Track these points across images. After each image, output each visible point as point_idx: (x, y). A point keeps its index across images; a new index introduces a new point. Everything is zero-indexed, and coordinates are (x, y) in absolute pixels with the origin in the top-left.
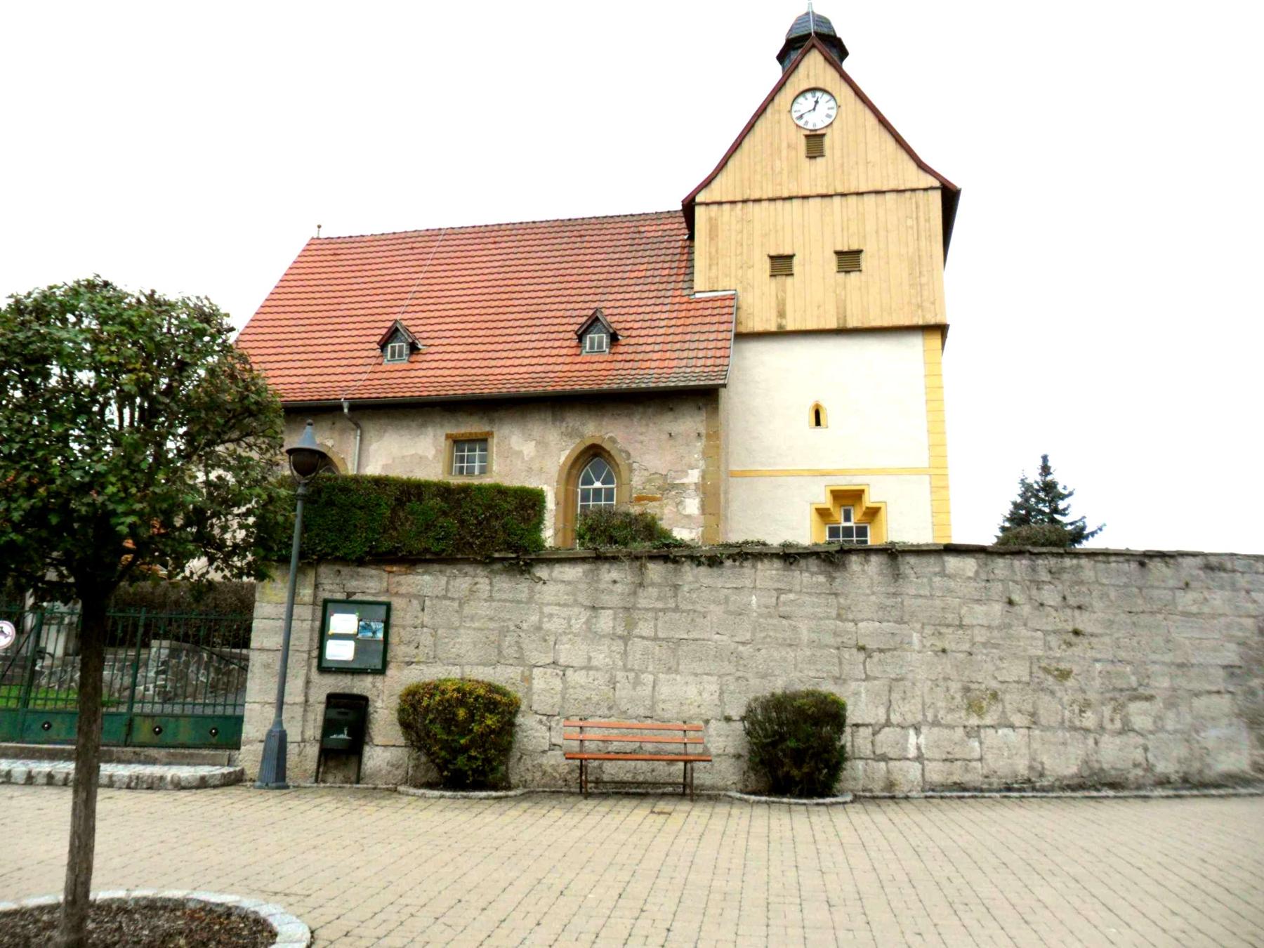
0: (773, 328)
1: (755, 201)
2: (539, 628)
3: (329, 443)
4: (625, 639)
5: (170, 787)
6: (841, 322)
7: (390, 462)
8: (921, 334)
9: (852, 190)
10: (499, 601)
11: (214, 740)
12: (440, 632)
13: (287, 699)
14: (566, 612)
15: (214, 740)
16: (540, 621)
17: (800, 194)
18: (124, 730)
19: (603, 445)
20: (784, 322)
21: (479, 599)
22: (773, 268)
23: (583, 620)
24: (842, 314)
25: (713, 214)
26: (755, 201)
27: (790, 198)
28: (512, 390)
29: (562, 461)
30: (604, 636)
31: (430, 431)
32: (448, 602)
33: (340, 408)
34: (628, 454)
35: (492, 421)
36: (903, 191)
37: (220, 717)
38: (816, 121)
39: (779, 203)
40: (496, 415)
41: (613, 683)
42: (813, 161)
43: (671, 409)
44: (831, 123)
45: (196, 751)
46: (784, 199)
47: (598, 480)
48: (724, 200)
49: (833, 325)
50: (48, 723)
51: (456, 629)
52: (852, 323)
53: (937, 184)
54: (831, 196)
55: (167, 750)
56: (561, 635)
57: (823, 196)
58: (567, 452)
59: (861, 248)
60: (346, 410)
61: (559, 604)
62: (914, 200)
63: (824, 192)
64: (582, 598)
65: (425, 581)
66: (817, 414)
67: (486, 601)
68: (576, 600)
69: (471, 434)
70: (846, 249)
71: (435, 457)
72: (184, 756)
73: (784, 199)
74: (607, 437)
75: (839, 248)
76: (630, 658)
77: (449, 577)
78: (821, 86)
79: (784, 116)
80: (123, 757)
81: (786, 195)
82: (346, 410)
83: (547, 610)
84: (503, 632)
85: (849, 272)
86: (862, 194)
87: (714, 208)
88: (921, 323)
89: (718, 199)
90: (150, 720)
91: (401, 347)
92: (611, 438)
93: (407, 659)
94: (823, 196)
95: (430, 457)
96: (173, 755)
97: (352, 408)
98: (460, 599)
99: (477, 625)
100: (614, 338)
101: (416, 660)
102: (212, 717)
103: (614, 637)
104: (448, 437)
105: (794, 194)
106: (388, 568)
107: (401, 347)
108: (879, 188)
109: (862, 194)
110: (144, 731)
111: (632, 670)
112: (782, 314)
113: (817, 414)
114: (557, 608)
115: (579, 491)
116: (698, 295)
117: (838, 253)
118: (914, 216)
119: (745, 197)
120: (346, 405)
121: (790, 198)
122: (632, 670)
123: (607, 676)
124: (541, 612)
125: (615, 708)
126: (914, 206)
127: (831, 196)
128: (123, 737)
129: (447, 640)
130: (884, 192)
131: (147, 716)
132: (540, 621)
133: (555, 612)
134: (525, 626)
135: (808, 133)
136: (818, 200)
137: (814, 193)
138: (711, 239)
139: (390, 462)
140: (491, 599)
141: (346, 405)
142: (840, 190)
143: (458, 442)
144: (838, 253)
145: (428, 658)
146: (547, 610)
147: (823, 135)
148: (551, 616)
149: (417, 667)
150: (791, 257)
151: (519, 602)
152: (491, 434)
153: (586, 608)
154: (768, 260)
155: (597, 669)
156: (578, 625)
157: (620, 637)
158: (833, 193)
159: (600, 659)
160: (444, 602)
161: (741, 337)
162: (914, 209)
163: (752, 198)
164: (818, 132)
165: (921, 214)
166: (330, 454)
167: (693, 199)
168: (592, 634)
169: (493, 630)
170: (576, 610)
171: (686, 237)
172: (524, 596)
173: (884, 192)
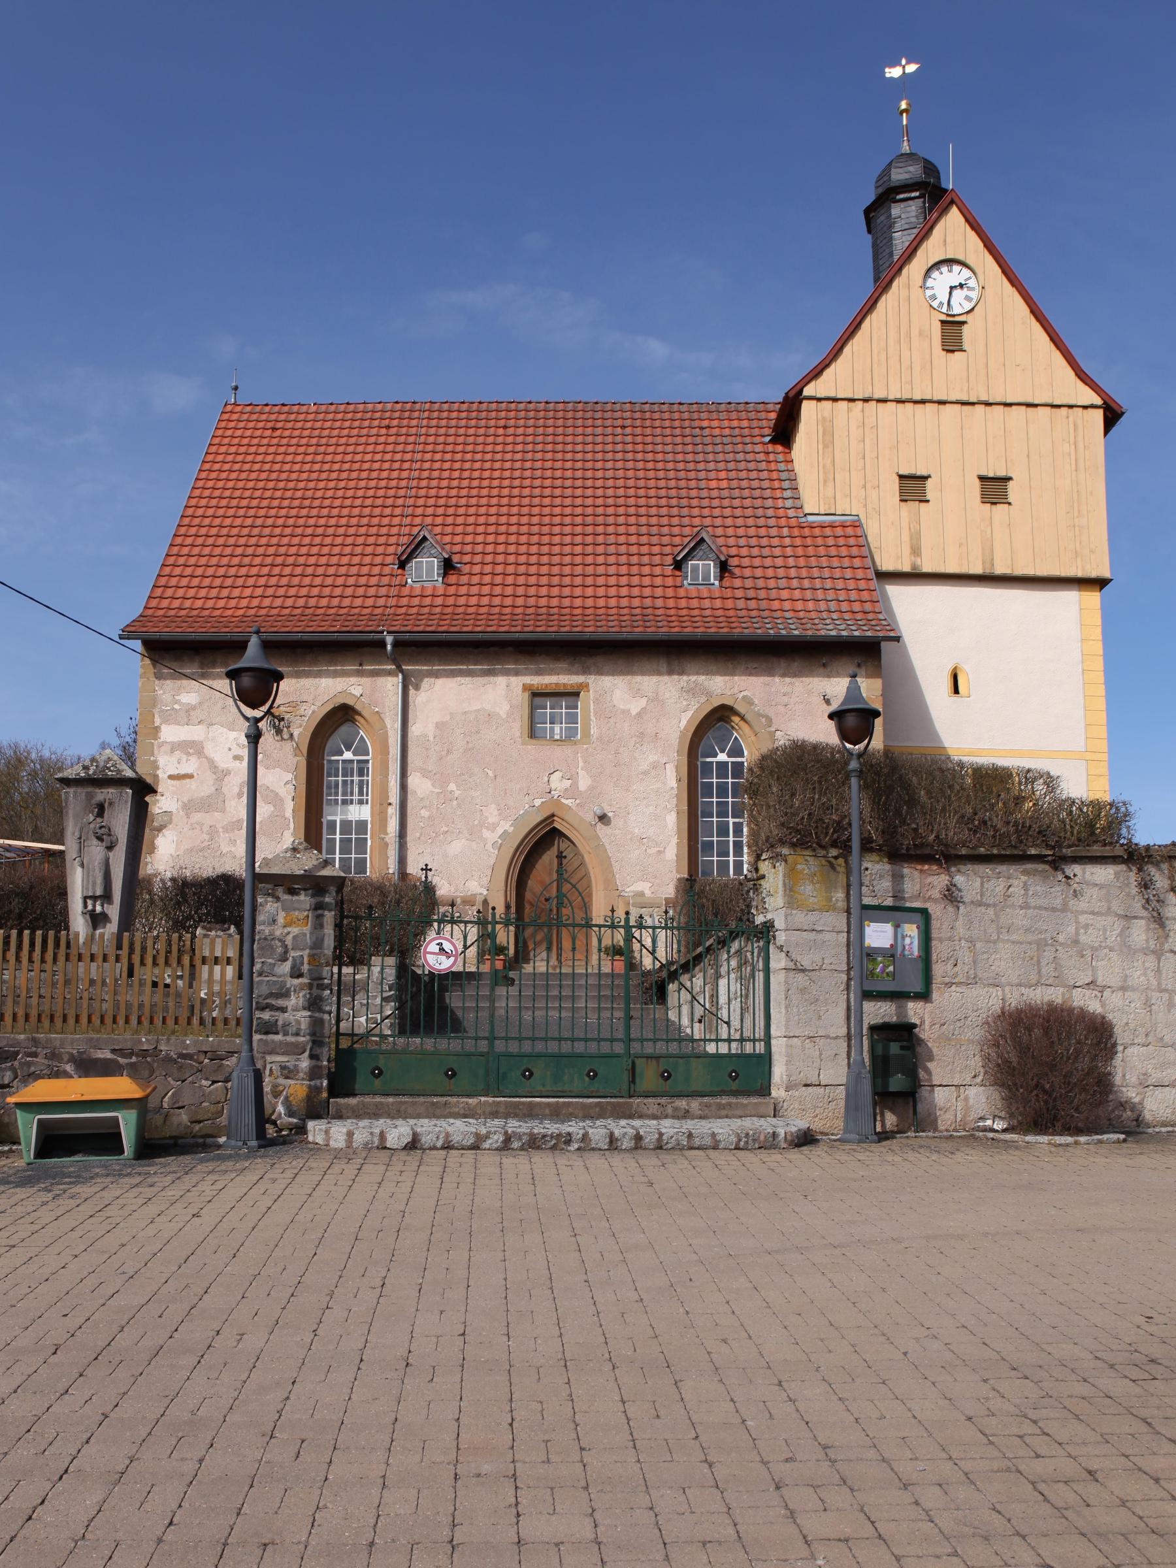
0: (907, 568)
1: (879, 401)
2: (1076, 942)
3: (357, 691)
4: (1158, 954)
5: (783, 1145)
6: (988, 566)
7: (447, 718)
8: (1076, 586)
9: (998, 400)
10: (1035, 908)
11: (734, 1086)
12: (978, 945)
13: (773, 1032)
14: (1100, 922)
15: (734, 1086)
16: (1077, 934)
17: (935, 399)
18: (625, 1077)
19: (736, 706)
20: (918, 562)
21: (1013, 906)
22: (902, 491)
23: (1118, 932)
24: (989, 554)
25: (827, 414)
26: (879, 401)
27: (923, 402)
28: (746, 631)
29: (684, 723)
30: (1136, 951)
31: (501, 681)
32: (983, 909)
33: (383, 644)
34: (770, 721)
35: (586, 671)
36: (1059, 406)
37: (737, 1056)
38: (960, 304)
39: (909, 406)
40: (590, 661)
41: (1148, 1005)
42: (950, 355)
43: (824, 665)
44: (972, 309)
45: (733, 1100)
46: (916, 402)
47: (722, 751)
48: (839, 396)
49: (977, 570)
50: (529, 1070)
51: (995, 942)
52: (999, 570)
53: (1099, 402)
54: (973, 404)
55: (700, 1100)
56: (1097, 949)
57: (964, 403)
58: (689, 714)
59: (1009, 475)
60: (389, 647)
61: (1093, 913)
62: (1071, 419)
63: (965, 398)
64: (1116, 906)
65: (968, 880)
66: (955, 678)
67: (1022, 908)
68: (1109, 908)
69: (556, 684)
70: (991, 475)
71: (509, 714)
72: (720, 1107)
73: (916, 402)
74: (741, 696)
75: (984, 473)
76: (1164, 975)
77: (982, 878)
78: (961, 257)
79: (916, 291)
80: (645, 1111)
81: (917, 397)
82: (389, 647)
83: (1083, 919)
84: (1041, 945)
85: (995, 503)
86: (1010, 405)
87: (828, 404)
88: (1080, 574)
89: (832, 394)
90: (654, 1062)
91: (430, 564)
92: (744, 697)
93: (947, 980)
94: (964, 403)
95: (503, 714)
96: (708, 1106)
97: (396, 644)
98: (995, 905)
99: (1015, 937)
100: (724, 568)
101: (956, 980)
102: (729, 1056)
103: (1146, 951)
104: (526, 688)
105: (928, 397)
106: (919, 867)
107: (430, 564)
108: (1030, 400)
109: (1010, 405)
110: (649, 1077)
111: (1166, 990)
112: (916, 551)
113: (955, 678)
114: (1091, 916)
115: (699, 763)
116: (810, 518)
117: (982, 478)
118: (1072, 440)
119: (867, 395)
120: (389, 640)
121: (923, 402)
122: (1166, 990)
123: (1143, 997)
124: (1077, 922)
125: (1152, 1034)
126: (1071, 426)
127: (973, 404)
128: (625, 1086)
129: (985, 956)
130: (1036, 406)
131: (649, 1057)
132: (1077, 934)
133: (1090, 922)
134: (1061, 938)
135: (944, 318)
136: (958, 407)
137: (953, 399)
138: (825, 446)
139: (447, 718)
140: (1026, 906)
141: (389, 640)
142: (984, 398)
143: (537, 695)
144: (982, 478)
145: (968, 978)
146: (1083, 919)
147: (964, 323)
148: (1086, 926)
149: (958, 989)
150: (925, 478)
151: (1054, 910)
152: (585, 686)
153: (1120, 916)
154: (897, 479)
155: (1134, 990)
156: (1113, 937)
157: (1153, 952)
158: (975, 400)
159: (1137, 977)
160: (979, 909)
161: (1100, 583)
162: (1072, 431)
163: (876, 396)
164: (957, 319)
165: (1080, 438)
166: (358, 707)
167: (801, 391)
168: (1128, 951)
169: (1030, 943)
170: (1110, 919)
171: (768, 439)
172: (1058, 903)
173: (1036, 406)
